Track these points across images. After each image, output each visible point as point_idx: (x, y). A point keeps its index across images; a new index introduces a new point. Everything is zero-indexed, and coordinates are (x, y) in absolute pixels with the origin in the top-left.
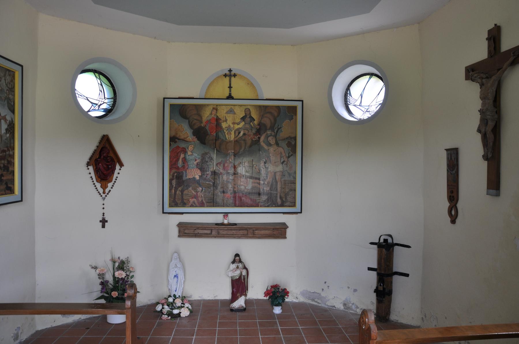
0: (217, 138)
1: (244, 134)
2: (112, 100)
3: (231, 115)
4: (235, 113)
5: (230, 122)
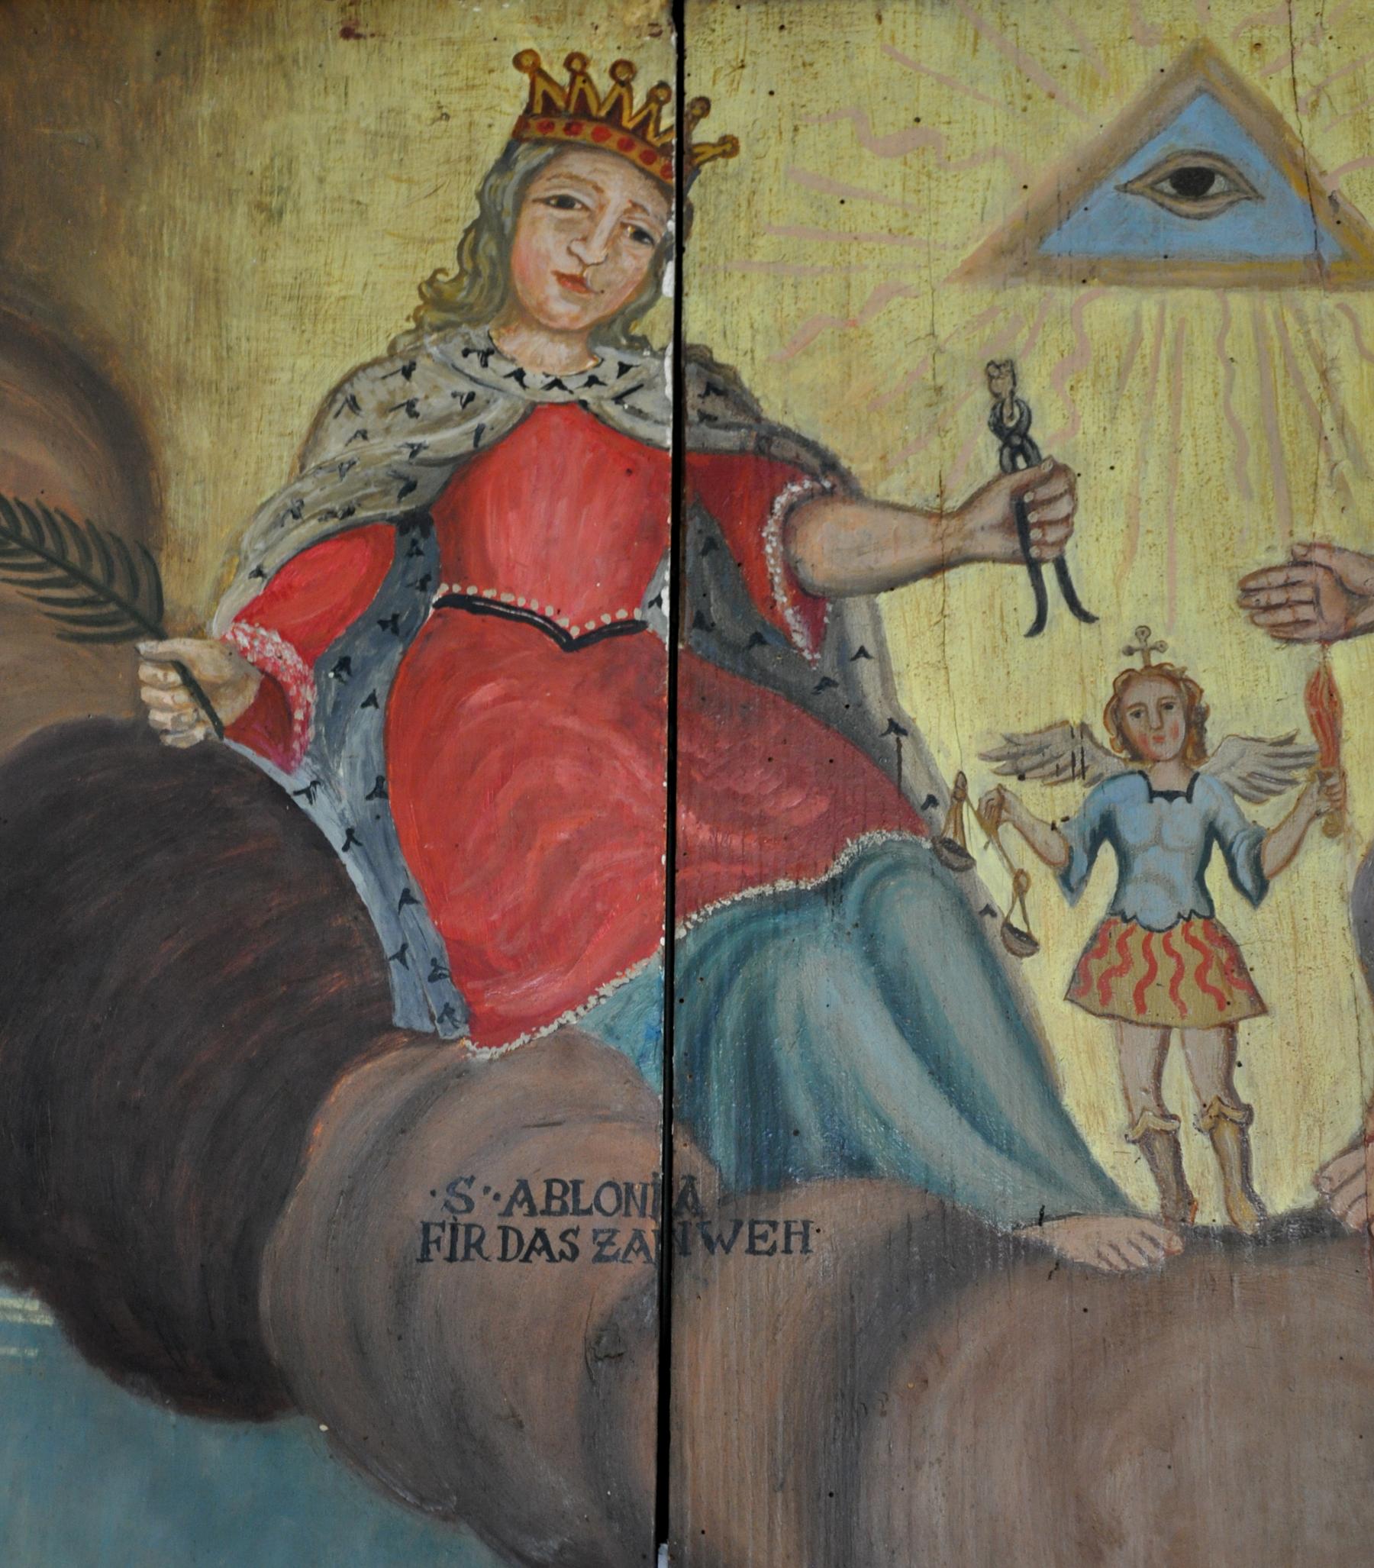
0: (726, 1138)
5: (1158, 569)
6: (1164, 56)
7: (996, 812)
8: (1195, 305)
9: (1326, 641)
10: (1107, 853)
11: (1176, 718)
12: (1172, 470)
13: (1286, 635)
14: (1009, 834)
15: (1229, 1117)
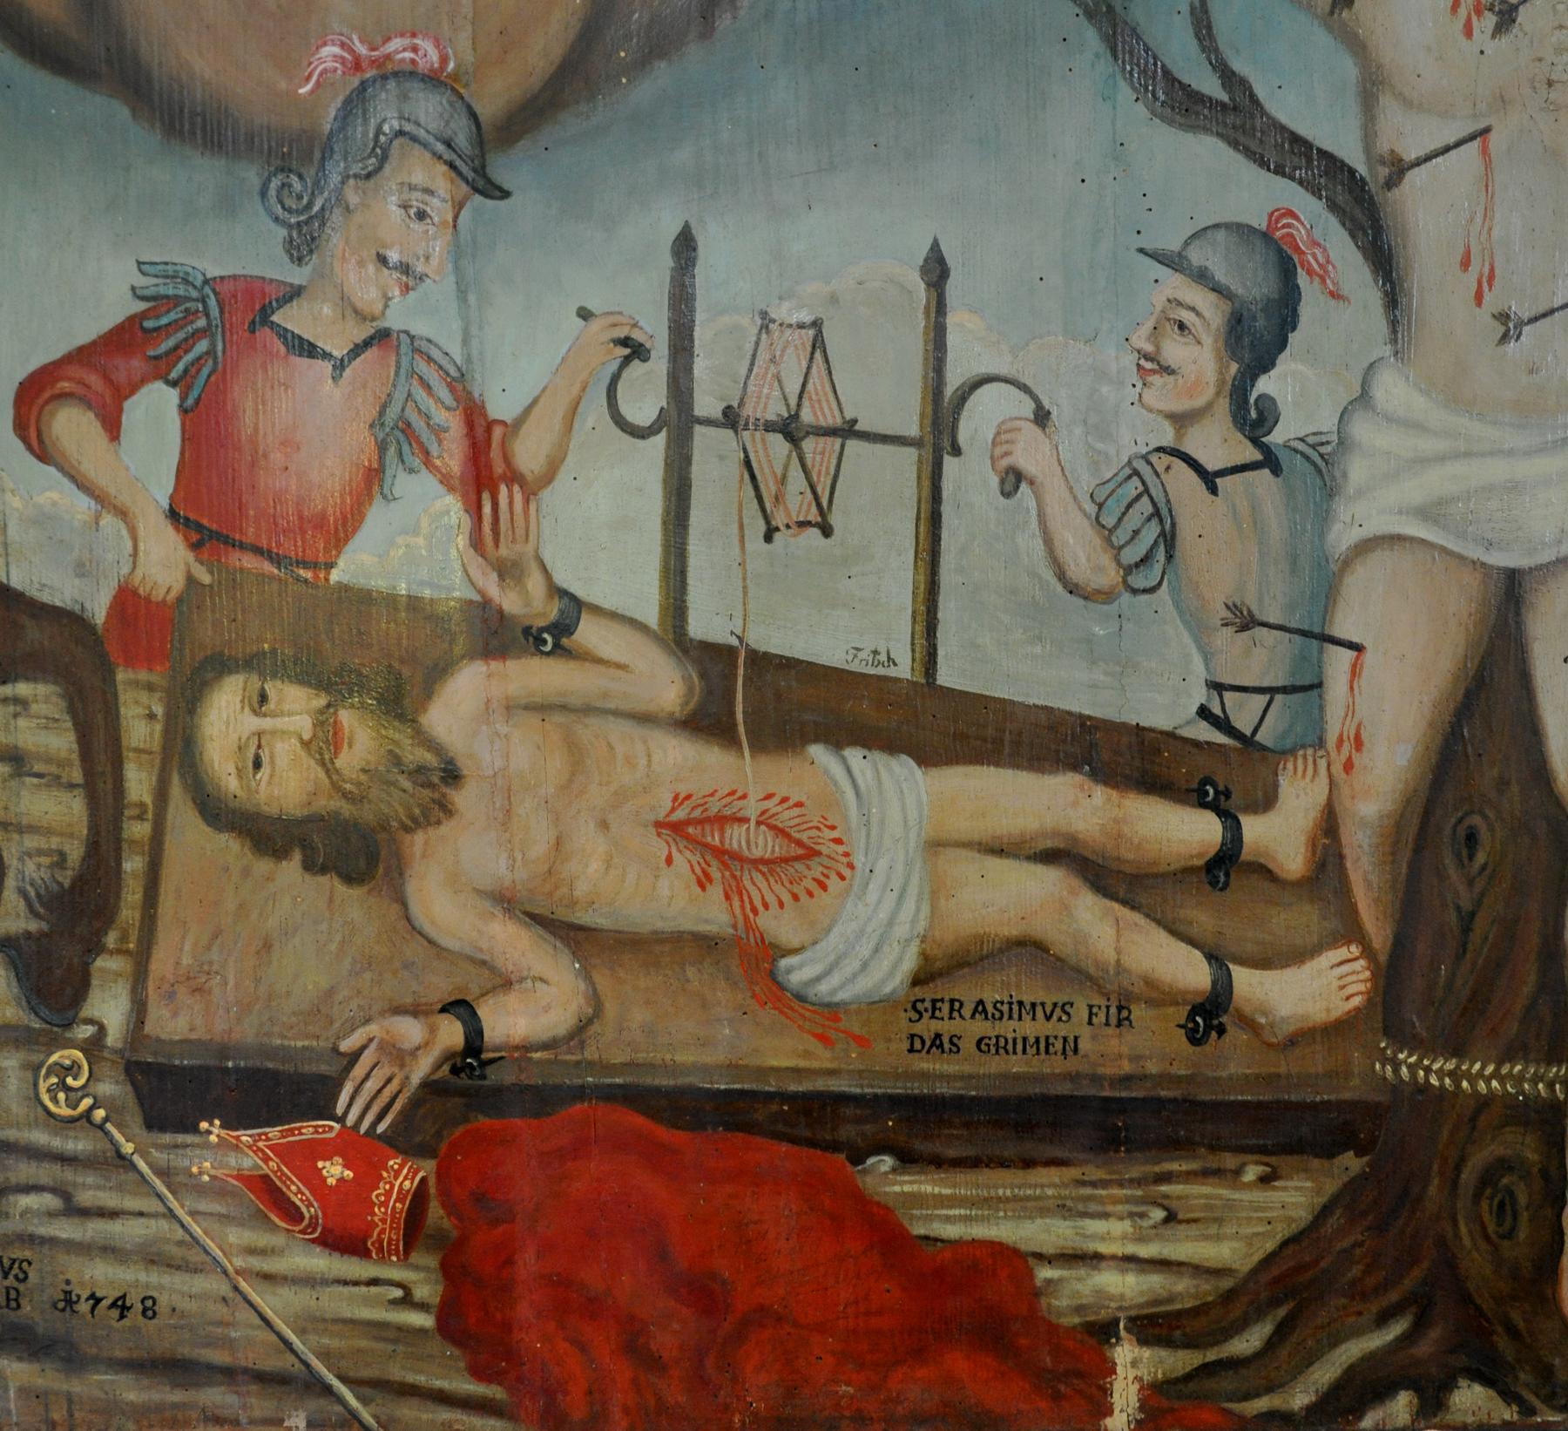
2: (839, 421)
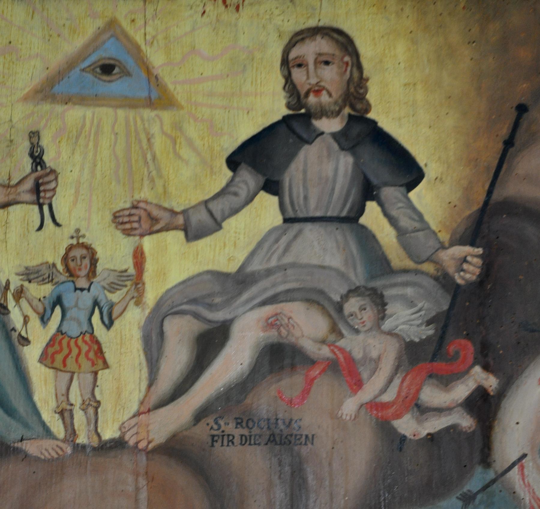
1: (278, 356)
3: (108, 119)
4: (159, 98)
5: (83, 209)
6: (100, 23)
7: (19, 294)
8: (105, 113)
9: (142, 236)
10: (58, 310)
11: (87, 262)
12: (93, 173)
13: (128, 233)
14: (24, 302)
15: (93, 405)
